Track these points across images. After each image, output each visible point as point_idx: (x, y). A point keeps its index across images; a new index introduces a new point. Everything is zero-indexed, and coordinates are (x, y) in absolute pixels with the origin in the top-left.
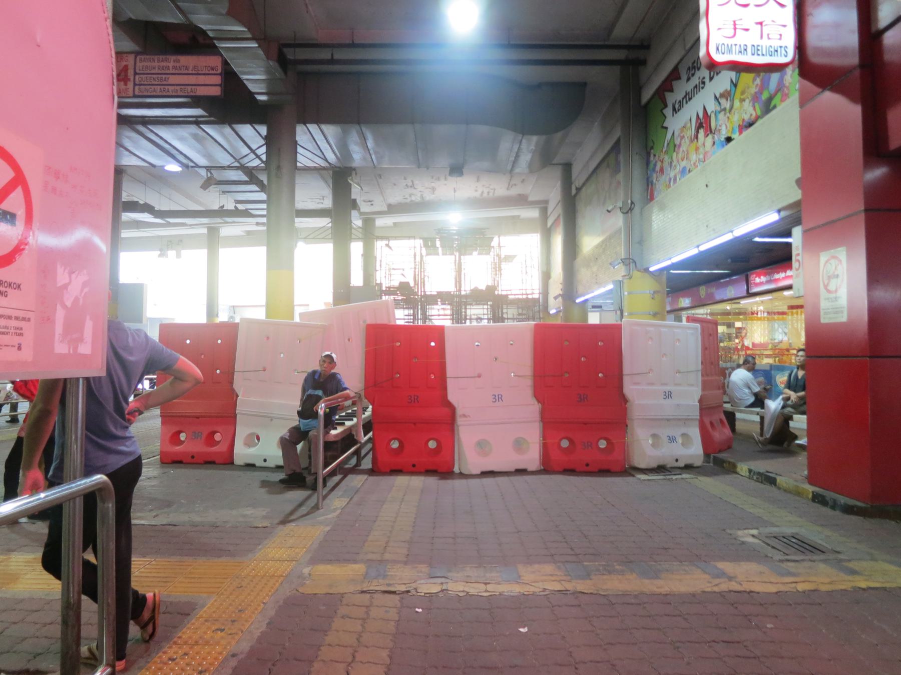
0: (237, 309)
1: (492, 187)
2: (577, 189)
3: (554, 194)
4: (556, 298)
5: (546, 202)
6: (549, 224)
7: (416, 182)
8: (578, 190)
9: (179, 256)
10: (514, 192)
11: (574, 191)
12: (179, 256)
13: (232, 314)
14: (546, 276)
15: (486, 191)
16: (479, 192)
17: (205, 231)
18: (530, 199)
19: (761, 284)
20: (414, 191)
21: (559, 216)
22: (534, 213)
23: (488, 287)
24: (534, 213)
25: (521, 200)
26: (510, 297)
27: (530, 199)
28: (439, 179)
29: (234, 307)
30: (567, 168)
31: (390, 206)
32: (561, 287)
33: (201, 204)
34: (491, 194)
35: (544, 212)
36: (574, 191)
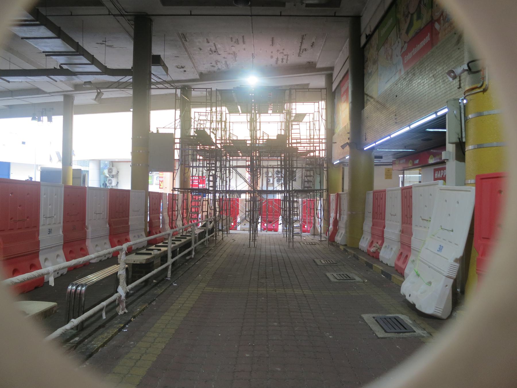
0: (114, 164)
1: (285, 53)
2: (367, 36)
3: (340, 59)
4: (343, 147)
5: (332, 69)
6: (334, 88)
7: (219, 46)
8: (369, 37)
9: (50, 120)
10: (305, 58)
11: (363, 40)
12: (50, 120)
13: (111, 167)
14: (331, 132)
15: (280, 57)
16: (274, 59)
17: (61, 99)
18: (319, 66)
19: (321, 182)
20: (218, 58)
21: (347, 72)
22: (320, 82)
23: (278, 136)
24: (320, 82)
25: (310, 68)
26: (300, 148)
27: (319, 66)
28: (237, 42)
29: (112, 162)
30: (356, 21)
31: (201, 74)
32: (349, 136)
33: (28, 61)
34: (285, 61)
35: (330, 78)
36: (363, 40)
